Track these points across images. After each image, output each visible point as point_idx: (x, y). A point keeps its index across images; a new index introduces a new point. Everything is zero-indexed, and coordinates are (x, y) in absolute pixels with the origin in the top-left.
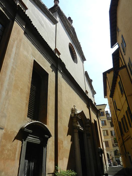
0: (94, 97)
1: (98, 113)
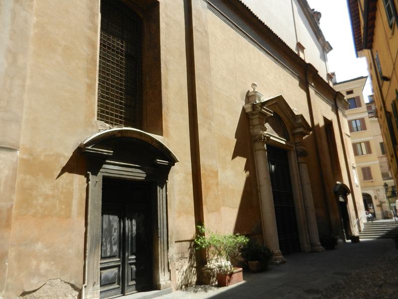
0: (324, 59)
1: (337, 99)
